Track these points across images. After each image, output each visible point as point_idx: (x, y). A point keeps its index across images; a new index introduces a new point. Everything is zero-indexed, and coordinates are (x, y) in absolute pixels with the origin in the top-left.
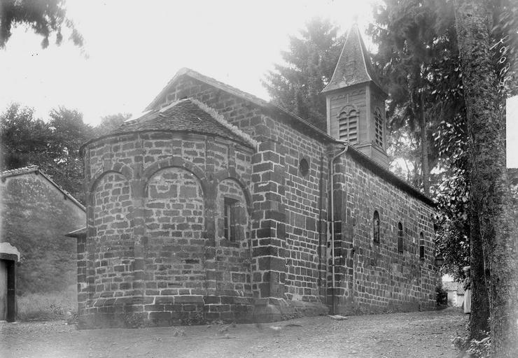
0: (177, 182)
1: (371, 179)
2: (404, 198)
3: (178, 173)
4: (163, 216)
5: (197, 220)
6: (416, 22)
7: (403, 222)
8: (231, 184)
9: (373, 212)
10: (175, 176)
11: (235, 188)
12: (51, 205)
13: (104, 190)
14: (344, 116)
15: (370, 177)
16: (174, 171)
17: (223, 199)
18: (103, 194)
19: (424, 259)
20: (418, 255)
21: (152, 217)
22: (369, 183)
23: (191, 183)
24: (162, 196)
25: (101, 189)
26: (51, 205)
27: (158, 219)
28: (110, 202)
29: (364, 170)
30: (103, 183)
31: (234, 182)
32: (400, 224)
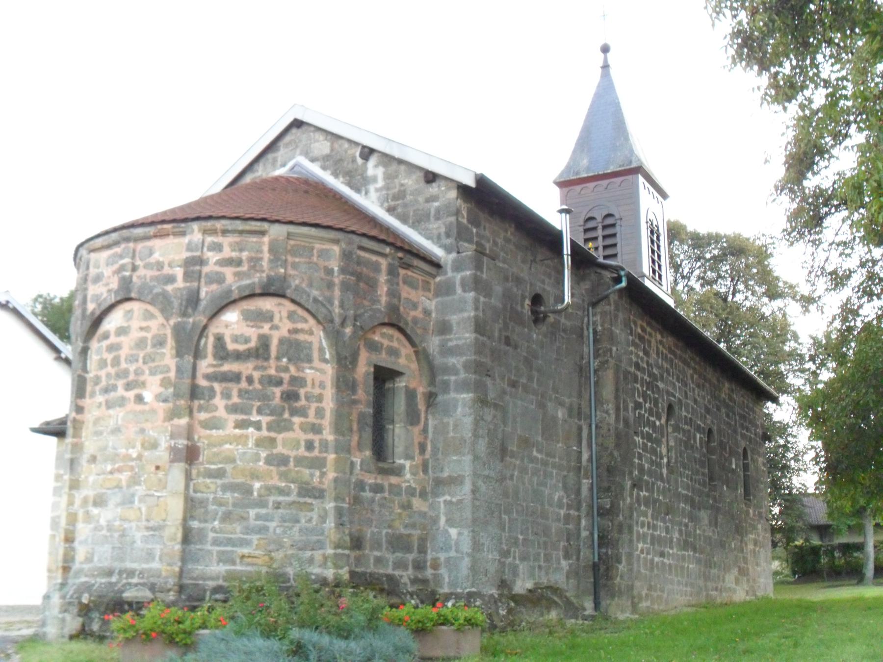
0: (271, 328)
1: (661, 342)
2: (714, 381)
3: (276, 310)
4: (235, 399)
5: (312, 412)
6: (756, 68)
7: (715, 428)
8: (391, 338)
9: (666, 405)
10: (268, 317)
11: (395, 344)
12: (699, 310)
13: (113, 339)
14: (590, 225)
15: (659, 337)
16: (267, 304)
17: (372, 370)
18: (111, 348)
19: (749, 500)
20: (741, 491)
21: (189, 327)
22: (657, 348)
23: (302, 331)
24: (238, 356)
25: (106, 336)
26: (699, 310)
27: (227, 407)
28: (124, 365)
29: (649, 324)
30: (111, 323)
31: (397, 334)
32: (710, 431)
